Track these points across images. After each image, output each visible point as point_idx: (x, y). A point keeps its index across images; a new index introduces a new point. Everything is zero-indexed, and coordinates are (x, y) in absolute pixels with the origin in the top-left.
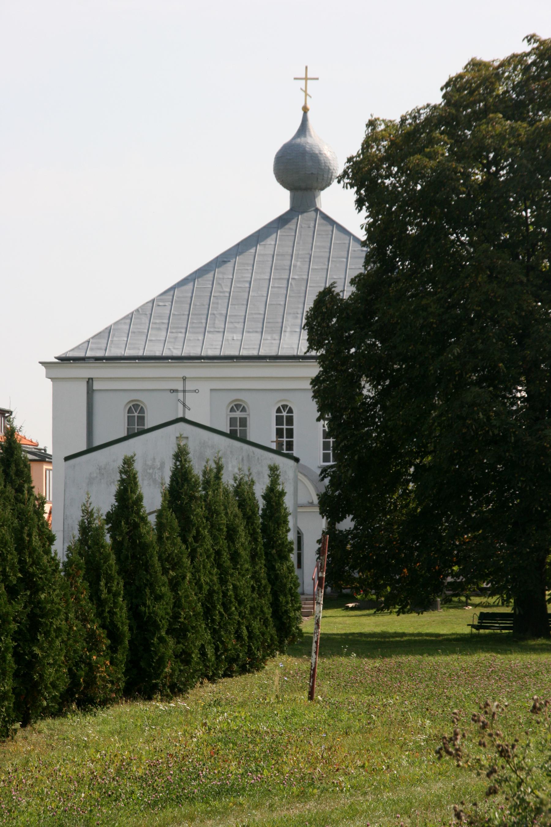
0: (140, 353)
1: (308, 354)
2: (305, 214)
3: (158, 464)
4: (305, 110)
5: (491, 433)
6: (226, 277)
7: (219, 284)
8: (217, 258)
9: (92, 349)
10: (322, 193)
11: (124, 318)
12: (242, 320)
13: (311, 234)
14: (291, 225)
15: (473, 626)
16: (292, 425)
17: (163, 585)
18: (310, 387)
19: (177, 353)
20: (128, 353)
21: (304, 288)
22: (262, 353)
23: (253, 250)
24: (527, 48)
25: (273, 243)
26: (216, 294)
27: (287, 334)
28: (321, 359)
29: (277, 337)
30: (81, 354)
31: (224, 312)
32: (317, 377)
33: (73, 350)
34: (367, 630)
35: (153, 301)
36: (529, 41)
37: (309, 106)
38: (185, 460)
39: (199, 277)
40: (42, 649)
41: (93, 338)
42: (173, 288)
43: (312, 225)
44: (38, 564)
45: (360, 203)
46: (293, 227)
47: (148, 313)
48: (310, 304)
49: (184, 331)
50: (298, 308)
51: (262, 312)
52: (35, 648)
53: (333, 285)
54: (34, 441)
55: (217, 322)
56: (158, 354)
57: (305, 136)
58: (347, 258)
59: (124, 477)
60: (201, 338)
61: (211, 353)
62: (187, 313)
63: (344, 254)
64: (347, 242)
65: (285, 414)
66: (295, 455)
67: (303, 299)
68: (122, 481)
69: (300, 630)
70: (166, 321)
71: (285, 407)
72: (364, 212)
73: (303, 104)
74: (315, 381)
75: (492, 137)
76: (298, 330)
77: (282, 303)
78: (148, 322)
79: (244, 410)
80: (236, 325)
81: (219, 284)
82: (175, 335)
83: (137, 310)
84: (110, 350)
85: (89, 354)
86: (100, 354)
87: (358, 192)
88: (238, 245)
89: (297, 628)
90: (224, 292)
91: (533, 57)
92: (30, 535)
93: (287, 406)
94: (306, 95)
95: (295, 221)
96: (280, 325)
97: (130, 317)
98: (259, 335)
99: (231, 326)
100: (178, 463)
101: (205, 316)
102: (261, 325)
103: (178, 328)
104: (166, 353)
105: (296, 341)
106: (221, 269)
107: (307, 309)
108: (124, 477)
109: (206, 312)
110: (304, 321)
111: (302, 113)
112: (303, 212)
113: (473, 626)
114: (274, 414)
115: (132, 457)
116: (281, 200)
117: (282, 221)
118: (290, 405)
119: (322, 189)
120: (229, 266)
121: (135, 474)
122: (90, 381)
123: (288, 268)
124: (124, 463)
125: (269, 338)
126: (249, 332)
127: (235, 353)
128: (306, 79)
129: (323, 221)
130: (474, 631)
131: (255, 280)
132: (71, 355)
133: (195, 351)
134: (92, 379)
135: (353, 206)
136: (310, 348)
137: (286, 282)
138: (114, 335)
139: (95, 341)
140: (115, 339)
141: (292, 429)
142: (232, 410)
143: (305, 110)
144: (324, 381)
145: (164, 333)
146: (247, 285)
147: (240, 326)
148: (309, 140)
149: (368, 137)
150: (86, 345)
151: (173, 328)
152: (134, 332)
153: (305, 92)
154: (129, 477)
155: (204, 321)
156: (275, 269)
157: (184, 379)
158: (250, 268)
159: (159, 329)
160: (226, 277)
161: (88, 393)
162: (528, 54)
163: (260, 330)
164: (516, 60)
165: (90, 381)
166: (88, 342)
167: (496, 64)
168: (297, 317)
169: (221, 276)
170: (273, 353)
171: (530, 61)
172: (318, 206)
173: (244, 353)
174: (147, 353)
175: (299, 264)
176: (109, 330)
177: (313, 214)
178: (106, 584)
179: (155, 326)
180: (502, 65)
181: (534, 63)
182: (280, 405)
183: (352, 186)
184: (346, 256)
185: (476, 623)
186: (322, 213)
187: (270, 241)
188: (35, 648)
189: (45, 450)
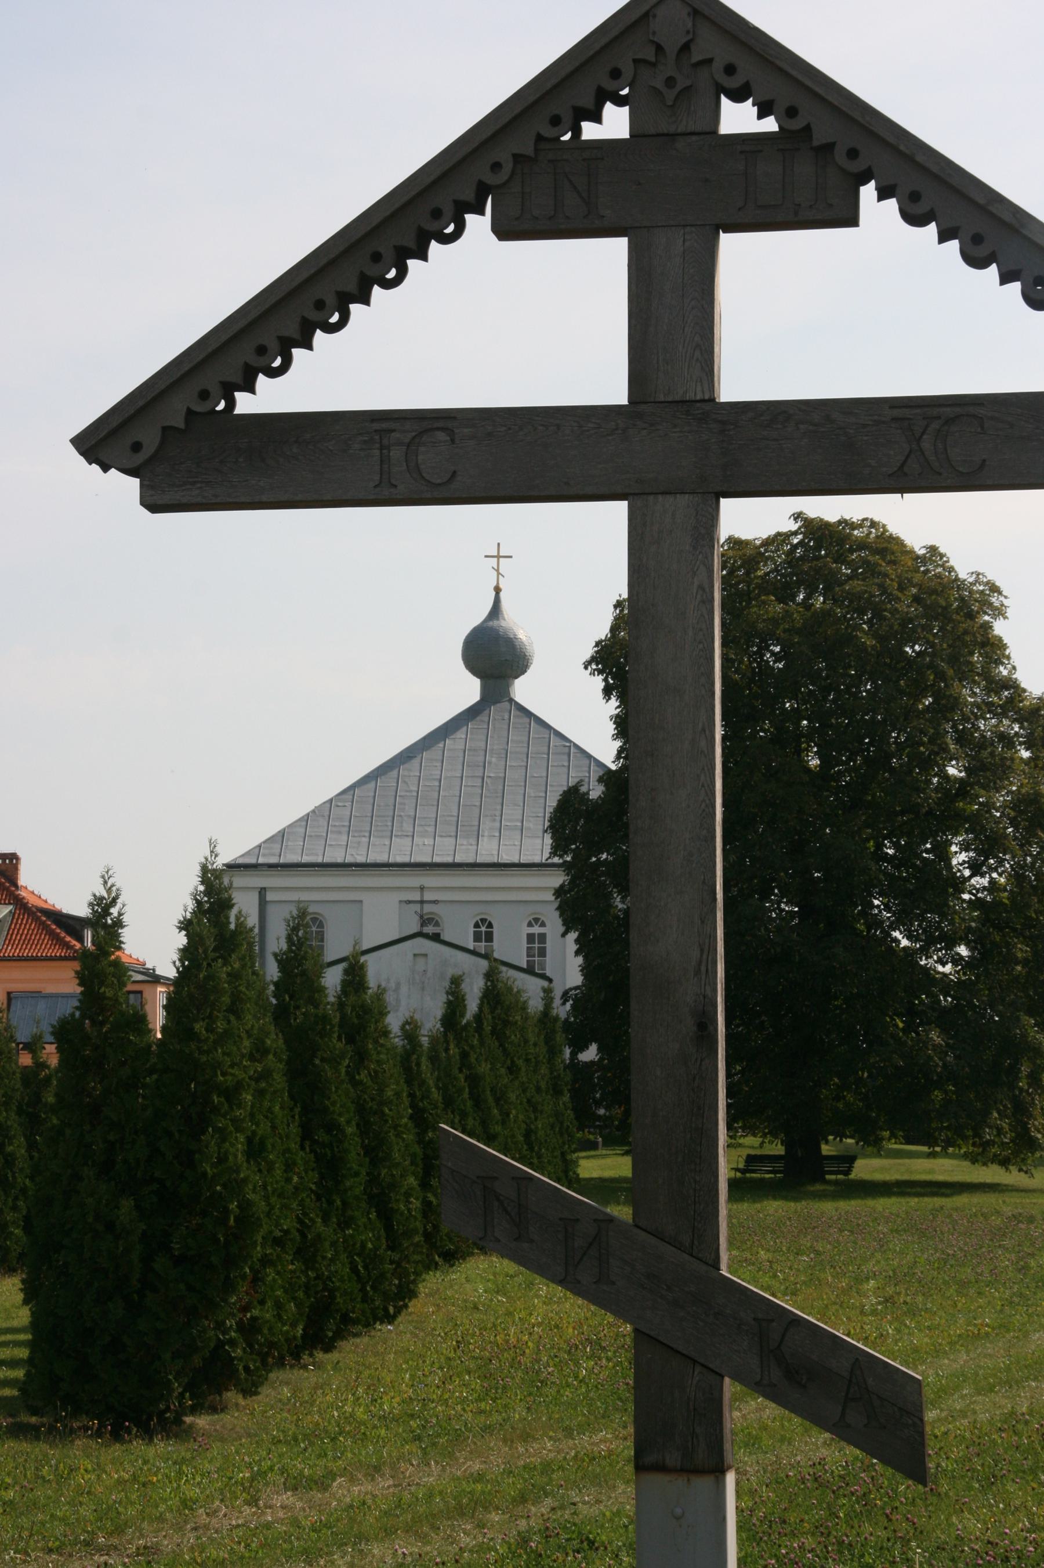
0: (319, 860)
1: (550, 861)
2: (498, 705)
3: (393, 985)
4: (497, 590)
5: (772, 951)
6: (412, 774)
7: (405, 782)
8: (402, 752)
9: (264, 855)
10: (516, 681)
11: (300, 820)
12: (433, 823)
13: (506, 727)
14: (483, 717)
15: (737, 1170)
16: (545, 943)
17: (497, 1123)
18: (553, 898)
19: (360, 859)
20: (306, 859)
21: (501, 787)
22: (458, 859)
23: (441, 745)
24: (793, 526)
25: (464, 736)
26: (403, 794)
27: (485, 839)
28: (566, 867)
29: (474, 842)
30: (252, 860)
31: (412, 814)
32: (562, 886)
33: (243, 856)
34: (608, 1174)
35: (331, 800)
36: (795, 519)
37: (501, 586)
38: (498, 980)
39: (381, 775)
40: (435, 1195)
41: (264, 842)
42: (352, 787)
43: (506, 717)
44: (428, 1097)
45: (607, 692)
46: (486, 719)
47: (327, 813)
48: (552, 802)
49: (367, 834)
50: (496, 810)
51: (456, 814)
52: (429, 1195)
53: (580, 783)
54: (141, 960)
55: (404, 824)
56: (340, 860)
57: (498, 619)
58: (548, 754)
59: (450, 998)
60: (387, 843)
61: (400, 859)
62: (370, 814)
63: (545, 749)
64: (547, 736)
65: (483, 929)
66: (548, 974)
67: (500, 800)
68: (449, 1003)
69: (578, 1175)
70: (347, 824)
71: (483, 920)
72: (614, 702)
73: (495, 584)
74: (559, 892)
75: (764, 621)
76: (541, 835)
77: (478, 804)
78: (326, 824)
79: (437, 924)
80: (427, 828)
81: (405, 782)
82: (357, 839)
83: (313, 811)
84: (285, 856)
85: (261, 860)
86: (273, 860)
87: (605, 680)
88: (424, 738)
89: (575, 1173)
90: (411, 791)
91: (800, 537)
92: (418, 1064)
93: (486, 920)
94: (499, 574)
95: (487, 712)
96: (476, 828)
97: (306, 818)
98: (453, 840)
99: (421, 829)
100: (489, 984)
101: (391, 819)
102: (454, 829)
103: (361, 831)
104: (349, 859)
105: (538, 847)
106: (406, 766)
107: (550, 810)
108: (450, 998)
109: (391, 813)
110: (547, 824)
111: (494, 593)
112: (495, 703)
113: (737, 1170)
114: (472, 930)
115: (461, 976)
116: (469, 690)
117: (472, 713)
118: (489, 919)
119: (516, 678)
120: (415, 762)
121: (463, 996)
122: (262, 892)
123: (482, 764)
124: (452, 983)
125: (465, 842)
126: (441, 836)
127: (427, 859)
128: (498, 557)
129: (518, 713)
130: (739, 1175)
131: (446, 778)
132: (240, 861)
133: (382, 858)
134: (265, 888)
135: (600, 695)
136: (554, 853)
137: (480, 780)
138: (288, 840)
139: (267, 845)
140: (290, 843)
141: (545, 948)
142: (530, 925)
143: (497, 590)
144: (569, 891)
145: (345, 838)
146: (437, 784)
147: (431, 829)
148: (503, 623)
149: (616, 619)
150: (257, 850)
151: (356, 831)
152: (310, 836)
153: (498, 570)
154: (457, 998)
155: (390, 824)
156: (468, 766)
157: (422, 889)
158: (439, 764)
159: (340, 833)
160: (412, 774)
161: (260, 905)
162: (795, 533)
163: (454, 834)
164: (779, 539)
165: (262, 892)
166: (260, 846)
167: (758, 542)
168: (494, 820)
169: (406, 773)
170: (470, 859)
171: (796, 541)
172: (512, 696)
173: (437, 859)
174: (327, 860)
175: (494, 760)
176: (282, 834)
177: (507, 704)
178: (460, 1122)
179: (334, 829)
180: (763, 544)
181: (801, 543)
182: (478, 918)
183: (600, 672)
184: (546, 751)
185: (741, 1166)
186: (517, 704)
187: (461, 734)
188: (429, 1195)
189: (154, 970)
